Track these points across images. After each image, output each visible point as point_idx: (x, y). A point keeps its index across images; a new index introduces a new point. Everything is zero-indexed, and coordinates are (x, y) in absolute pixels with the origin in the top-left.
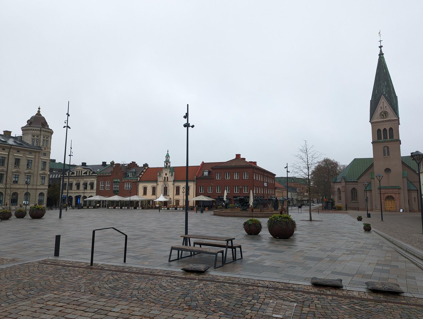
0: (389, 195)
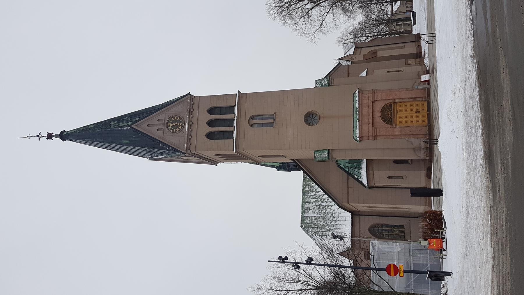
0: (378, 114)
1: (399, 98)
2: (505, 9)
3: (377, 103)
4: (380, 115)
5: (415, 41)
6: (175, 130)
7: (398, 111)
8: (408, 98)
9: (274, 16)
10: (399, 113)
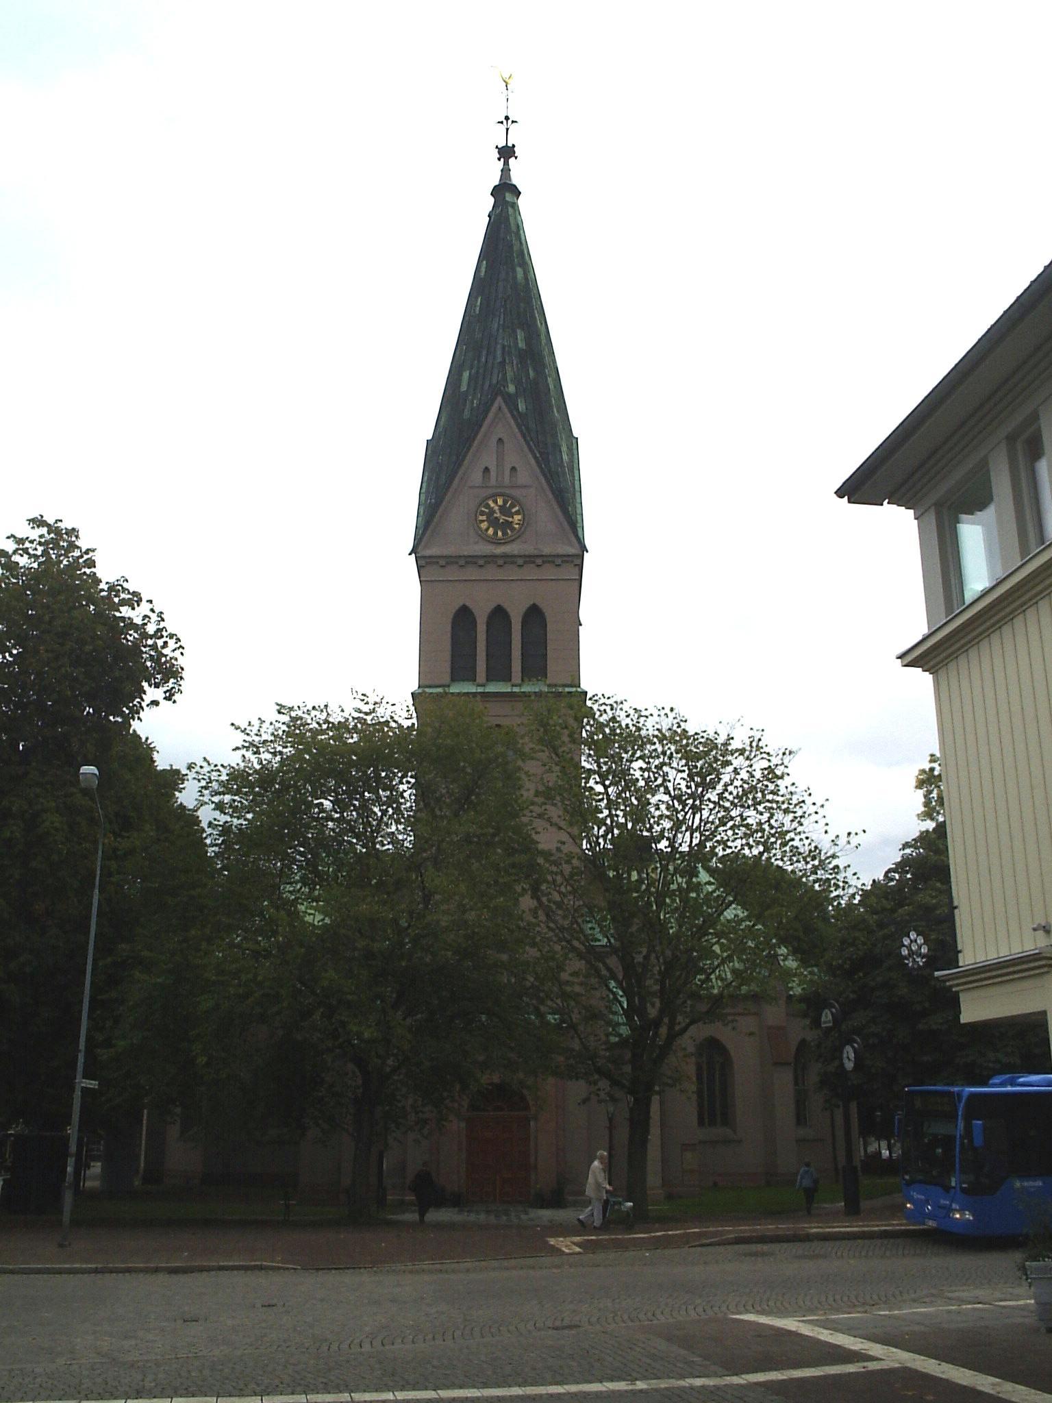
2: (678, 1232)
6: (484, 518)
9: (564, 822)
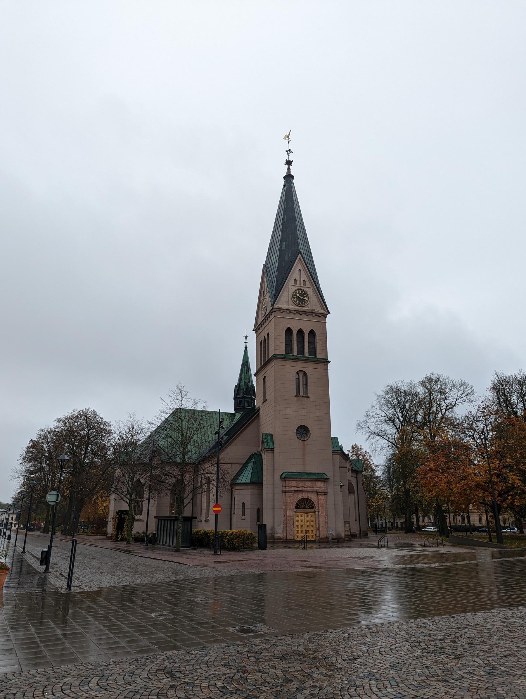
0: (305, 496)
1: (320, 515)
3: (316, 495)
4: (305, 497)
5: (360, 531)
7: (307, 514)
8: (319, 524)
10: (306, 515)
